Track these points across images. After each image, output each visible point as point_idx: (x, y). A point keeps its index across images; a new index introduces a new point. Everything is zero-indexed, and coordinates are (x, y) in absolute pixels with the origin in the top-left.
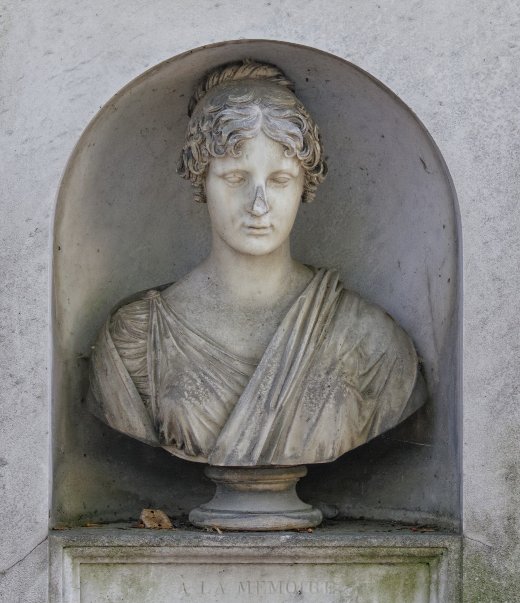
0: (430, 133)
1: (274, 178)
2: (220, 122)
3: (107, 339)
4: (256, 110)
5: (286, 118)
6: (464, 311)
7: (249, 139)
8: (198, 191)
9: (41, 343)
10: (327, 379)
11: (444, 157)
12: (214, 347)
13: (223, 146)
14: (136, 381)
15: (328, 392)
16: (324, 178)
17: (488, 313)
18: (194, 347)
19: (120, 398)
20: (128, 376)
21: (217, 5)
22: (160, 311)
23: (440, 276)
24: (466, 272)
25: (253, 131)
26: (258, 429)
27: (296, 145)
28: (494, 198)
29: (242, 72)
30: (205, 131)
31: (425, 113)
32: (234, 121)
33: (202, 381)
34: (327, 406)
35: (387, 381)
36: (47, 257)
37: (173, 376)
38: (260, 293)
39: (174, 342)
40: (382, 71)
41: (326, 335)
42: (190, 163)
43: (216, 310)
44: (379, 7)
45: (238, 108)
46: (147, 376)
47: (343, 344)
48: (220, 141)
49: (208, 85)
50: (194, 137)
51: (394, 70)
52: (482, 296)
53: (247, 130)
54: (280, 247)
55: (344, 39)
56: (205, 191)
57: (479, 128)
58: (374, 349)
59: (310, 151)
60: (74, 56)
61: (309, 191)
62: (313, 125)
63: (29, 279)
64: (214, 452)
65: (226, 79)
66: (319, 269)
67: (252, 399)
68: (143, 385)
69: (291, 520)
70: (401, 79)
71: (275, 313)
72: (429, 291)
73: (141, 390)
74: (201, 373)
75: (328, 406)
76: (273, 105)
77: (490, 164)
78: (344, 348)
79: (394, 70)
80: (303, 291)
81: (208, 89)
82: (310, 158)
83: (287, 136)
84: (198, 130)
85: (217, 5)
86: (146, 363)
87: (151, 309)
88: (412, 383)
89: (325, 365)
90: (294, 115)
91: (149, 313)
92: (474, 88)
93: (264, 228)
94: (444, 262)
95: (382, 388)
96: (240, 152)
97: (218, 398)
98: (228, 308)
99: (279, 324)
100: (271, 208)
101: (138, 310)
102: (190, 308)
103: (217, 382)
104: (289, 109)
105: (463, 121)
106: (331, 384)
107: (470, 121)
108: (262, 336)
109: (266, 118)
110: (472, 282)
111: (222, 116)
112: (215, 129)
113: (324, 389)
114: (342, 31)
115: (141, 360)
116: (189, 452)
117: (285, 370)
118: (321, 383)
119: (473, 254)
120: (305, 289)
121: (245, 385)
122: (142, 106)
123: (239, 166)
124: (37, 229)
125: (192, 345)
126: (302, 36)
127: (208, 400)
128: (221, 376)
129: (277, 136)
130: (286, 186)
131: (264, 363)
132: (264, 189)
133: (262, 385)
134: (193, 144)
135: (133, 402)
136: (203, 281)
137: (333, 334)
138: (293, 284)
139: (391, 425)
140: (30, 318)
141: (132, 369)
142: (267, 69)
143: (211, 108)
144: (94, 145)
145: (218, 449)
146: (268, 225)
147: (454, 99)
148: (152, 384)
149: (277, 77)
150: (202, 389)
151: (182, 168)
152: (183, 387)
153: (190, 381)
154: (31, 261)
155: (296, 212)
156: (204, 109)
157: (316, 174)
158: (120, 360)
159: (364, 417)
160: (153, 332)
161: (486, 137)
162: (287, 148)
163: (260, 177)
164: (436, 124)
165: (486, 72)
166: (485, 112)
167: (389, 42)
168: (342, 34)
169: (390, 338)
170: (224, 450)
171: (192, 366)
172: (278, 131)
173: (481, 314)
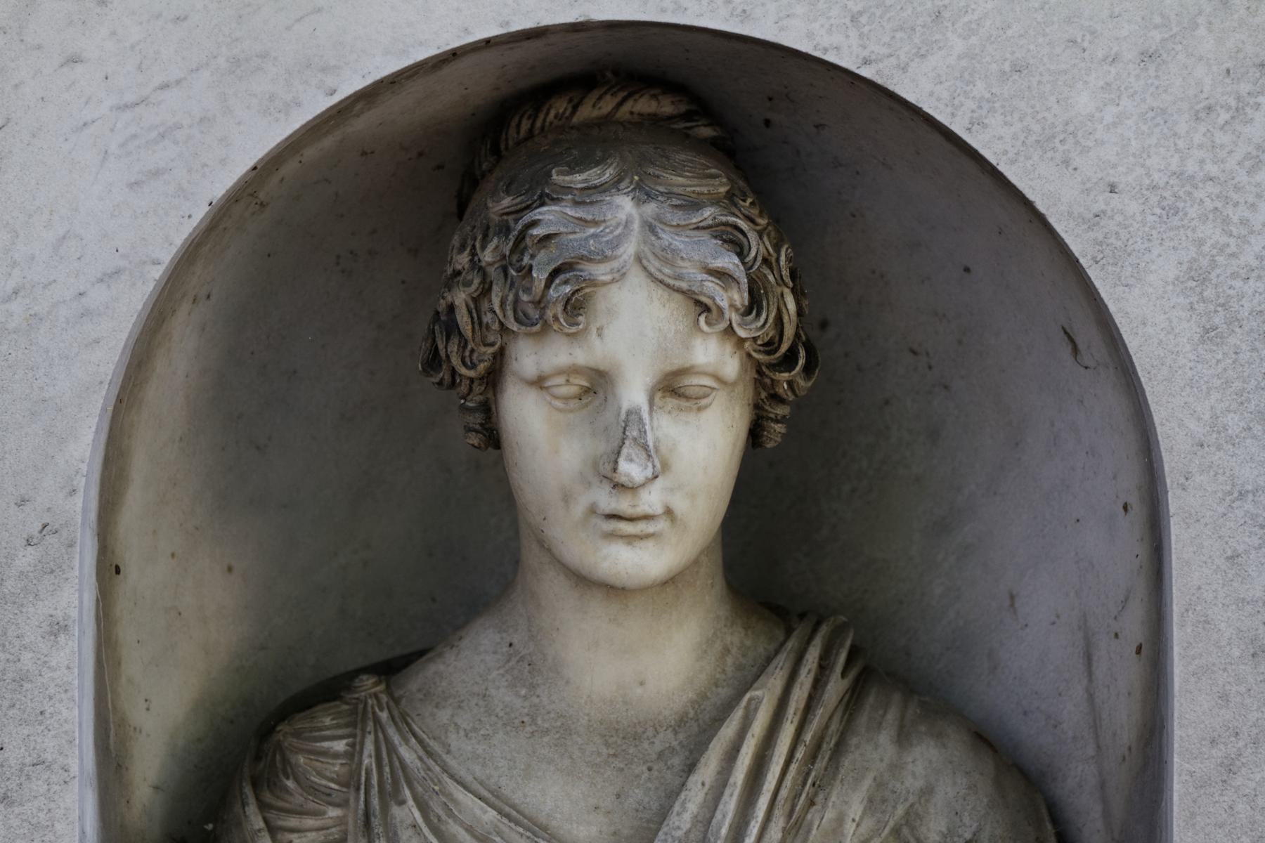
0: (1085, 265)
1: (673, 387)
2: (528, 241)
3: (244, 805)
4: (624, 207)
5: (704, 228)
6: (1176, 738)
7: (605, 284)
8: (476, 419)
9: (58, 826)
11: (1122, 331)
12: (521, 830)
16: (810, 384)
17: (1241, 744)
18: (467, 830)
22: (384, 732)
23: (1116, 635)
24: (1180, 635)
25: (615, 264)
27: (731, 299)
28: (1254, 437)
29: (594, 106)
31: (1070, 214)
32: (564, 238)
36: (74, 596)
38: (642, 684)
39: (417, 814)
40: (956, 102)
41: (816, 794)
42: (454, 347)
43: (528, 729)
45: (577, 204)
47: (862, 818)
48: (528, 290)
49: (507, 140)
50: (461, 278)
52: (1225, 697)
53: (600, 262)
54: (696, 562)
55: (854, 19)
56: (494, 419)
57: (1214, 252)
58: (944, 829)
60: (139, 68)
62: (777, 248)
63: (27, 657)
65: (551, 123)
66: (802, 616)
70: (1006, 124)
71: (681, 736)
72: (1090, 674)
76: (669, 195)
77: (1244, 347)
78: (863, 829)
80: (757, 677)
81: (507, 148)
83: (705, 276)
84: (471, 260)
87: (359, 726)
90: (724, 219)
91: (354, 736)
92: (1200, 146)
93: (647, 518)
94: (1127, 599)
96: (580, 318)
98: (559, 724)
99: (690, 768)
100: (666, 466)
101: (328, 728)
104: (712, 204)
105: (1172, 234)
107: (1189, 233)
108: (647, 799)
109: (650, 228)
110: (1196, 662)
111: (534, 224)
119: (1199, 588)
120: (762, 672)
122: (337, 194)
123: (579, 355)
124: (45, 526)
125: (462, 824)
126: (744, 11)
129: (679, 277)
130: (706, 407)
132: (645, 416)
134: (460, 297)
136: (495, 653)
137: (835, 793)
138: (729, 660)
140: (28, 760)
143: (507, 202)
144: (208, 297)
147: (1148, 175)
149: (687, 116)
151: (434, 361)
154: (31, 610)
155: (735, 473)
157: (786, 375)
160: (363, 787)
161: (1234, 275)
162: (707, 309)
163: (638, 382)
164: (1101, 244)
165: (1233, 103)
166: (1229, 211)
172: (681, 263)
173: (1222, 747)
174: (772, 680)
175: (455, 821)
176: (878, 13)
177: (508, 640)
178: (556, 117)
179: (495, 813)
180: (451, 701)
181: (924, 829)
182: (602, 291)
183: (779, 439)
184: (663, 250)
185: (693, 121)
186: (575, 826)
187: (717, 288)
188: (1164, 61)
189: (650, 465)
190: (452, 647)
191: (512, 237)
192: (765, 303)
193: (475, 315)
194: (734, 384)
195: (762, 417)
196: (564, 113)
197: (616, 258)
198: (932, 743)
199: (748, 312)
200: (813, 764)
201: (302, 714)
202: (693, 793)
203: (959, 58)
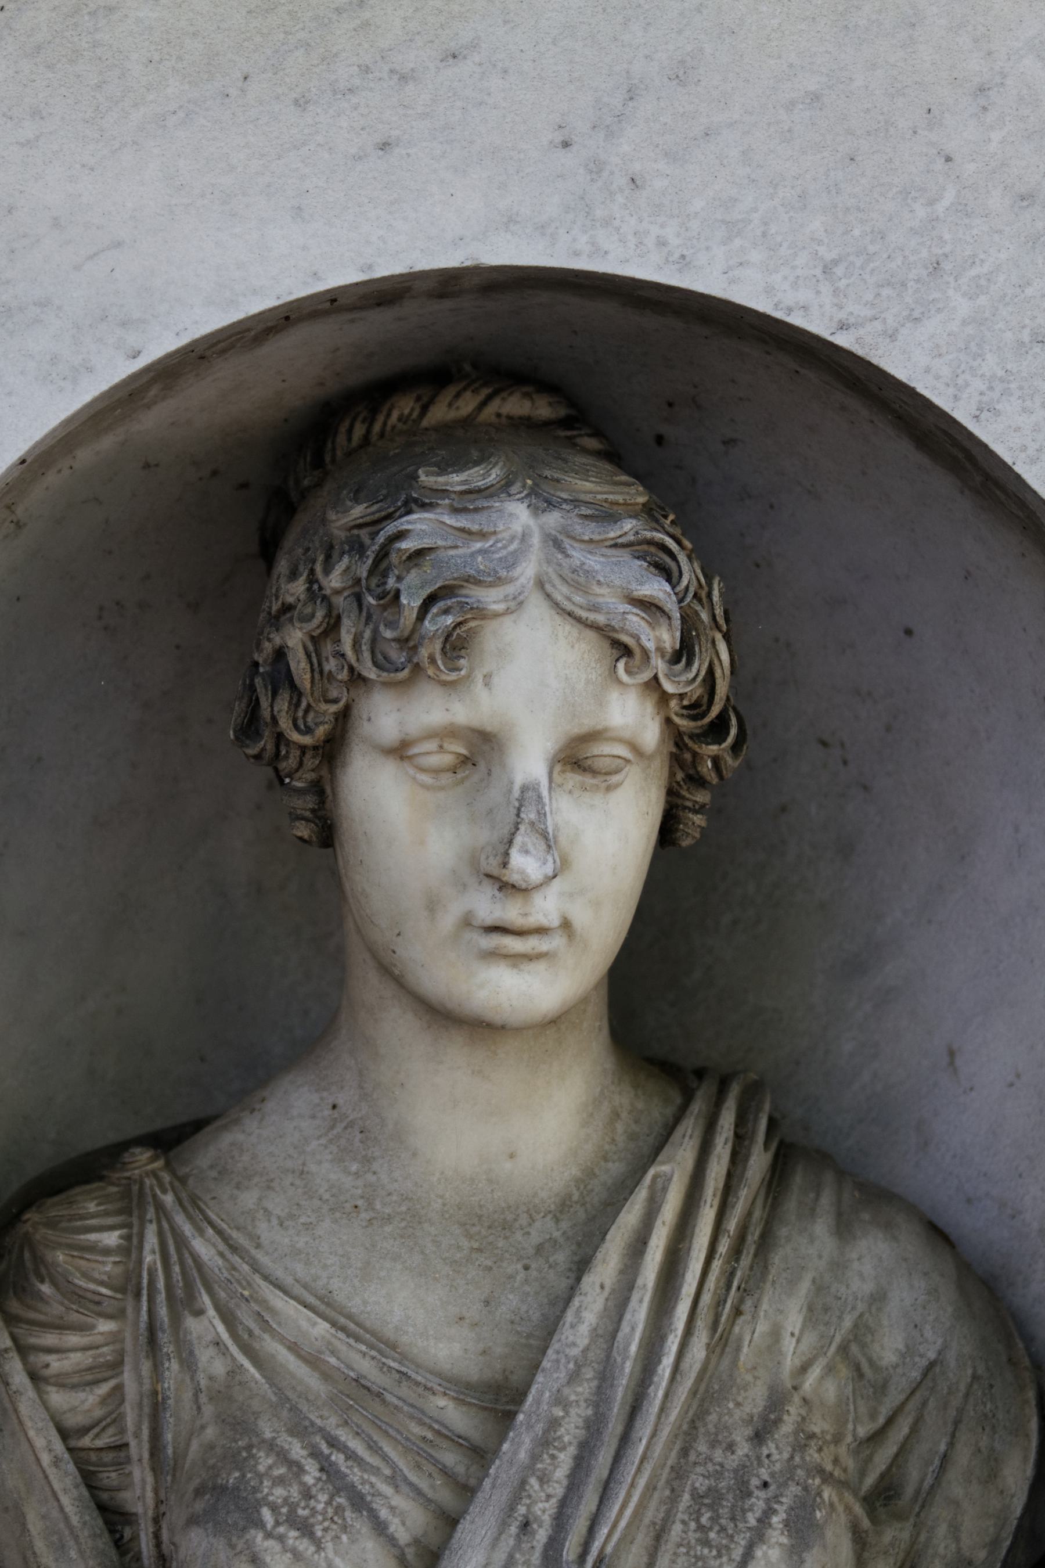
1: (576, 758)
2: (394, 558)
5: (624, 546)
7: (497, 615)
8: (305, 804)
10: (758, 1458)
12: (364, 1348)
13: (403, 642)
14: (88, 1462)
15: (761, 1505)
16: (737, 764)
18: (289, 1348)
19: (30, 1527)
20: (59, 1446)
21: (384, 146)
22: (169, 1220)
25: (510, 589)
29: (450, 405)
30: (337, 592)
32: (442, 554)
33: (322, 1469)
34: (759, 1553)
35: (945, 1458)
37: (219, 1451)
38: (512, 1156)
39: (221, 1328)
40: (960, 381)
41: (741, 1301)
42: (283, 704)
43: (364, 1215)
44: (948, 159)
45: (456, 511)
46: (126, 1445)
49: (334, 449)
51: (1002, 380)
53: (491, 585)
54: (584, 1000)
55: (827, 270)
56: (327, 806)
58: (901, 1346)
59: (699, 667)
61: (685, 808)
65: (394, 427)
66: (700, 1074)
67: (500, 1534)
68: (110, 1477)
70: (1024, 410)
71: (565, 1225)
73: (105, 1496)
74: (318, 1439)
75: (765, 1554)
76: (576, 502)
78: (804, 1346)
79: (1002, 380)
81: (333, 461)
82: (695, 691)
83: (628, 608)
84: (309, 589)
85: (384, 146)
87: (136, 1213)
88: (1025, 1459)
89: (748, 1410)
90: (648, 535)
91: (129, 1226)
93: (541, 931)
95: (929, 1480)
96: (462, 661)
97: (380, 1528)
98: (404, 1208)
99: (582, 1266)
101: (93, 1216)
102: (270, 1206)
103: (376, 1471)
104: (630, 517)
106: (772, 1475)
108: (524, 1308)
109: (555, 542)
111: (401, 535)
112: (374, 581)
113: (750, 1494)
114: (820, 242)
115: (104, 1389)
117: (614, 1427)
118: (735, 1471)
121: (472, 1482)
125: (282, 1340)
126: (683, 257)
128: (387, 1448)
129: (595, 608)
130: (617, 786)
131: (538, 1402)
132: (545, 793)
133: (533, 1481)
135: (76, 1538)
136: (313, 1117)
137: (765, 1299)
138: (620, 1127)
141: (72, 1421)
142: (534, 396)
143: (358, 511)
146: (553, 920)
148: (141, 1474)
149: (566, 423)
150: (323, 1498)
151: (251, 725)
152: (255, 1490)
153: (281, 1471)
156: (332, 516)
158: (31, 1393)
160: (145, 1292)
167: (983, 282)
168: (822, 250)
169: (950, 1309)
171: (285, 1414)
172: (597, 590)
174: (681, 1152)
175: (273, 1337)
176: (858, 262)
177: (331, 1101)
178: (400, 419)
179: (327, 1326)
180: (256, 1179)
181: (876, 1347)
182: (491, 625)
183: (698, 835)
184: (574, 571)
185: (572, 428)
186: (432, 1342)
187: (643, 624)
189: (550, 859)
190: (253, 1111)
191: (371, 555)
192: (697, 649)
193: (315, 660)
194: (650, 758)
195: (677, 806)
196: (410, 414)
197: (511, 580)
198: (881, 1235)
199: (676, 658)
200: (737, 1260)
201: (56, 1199)
202: (589, 1298)
203: (964, 323)
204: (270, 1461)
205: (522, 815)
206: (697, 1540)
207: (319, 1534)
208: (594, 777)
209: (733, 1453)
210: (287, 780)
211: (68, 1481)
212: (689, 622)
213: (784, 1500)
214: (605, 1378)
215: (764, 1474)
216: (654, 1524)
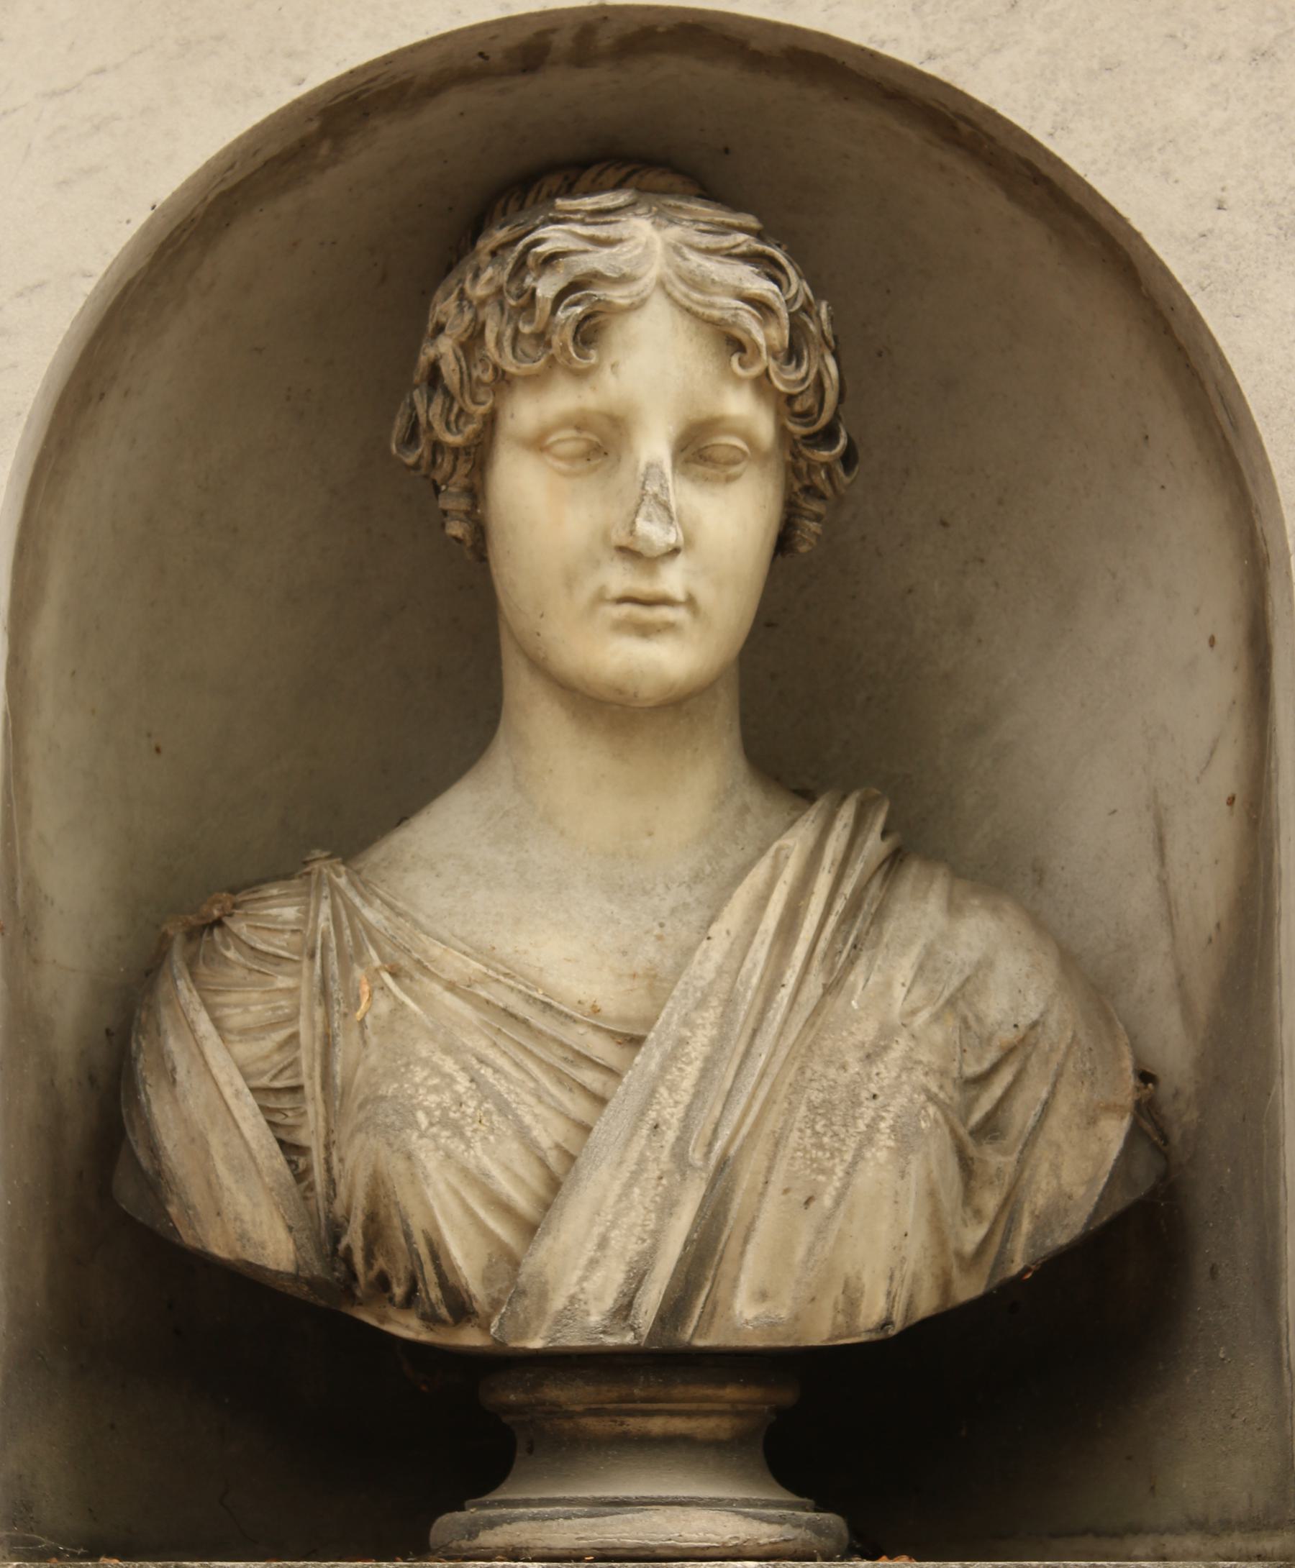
1: (698, 448)
2: (531, 261)
19: (213, 1152)
20: (240, 1082)
26: (651, 1226)
33: (472, 1080)
47: (913, 982)
64: (510, 1303)
67: (633, 1135)
69: (756, 1524)
86: (298, 1047)
93: (666, 601)
96: (593, 352)
106: (881, 1088)
113: (860, 1104)
116: (432, 1306)
127: (492, 1138)
131: (668, 1024)
139: (1062, 1237)
145: (522, 1293)
146: (680, 595)
147: (1262, 189)
150: (473, 1103)
153: (436, 1081)
155: (760, 592)
159: (978, 1213)
164: (1207, 268)
170: (543, 1296)
188: (1279, 61)
192: (805, 353)
204: (425, 1074)
205: (648, 488)
206: (812, 1145)
207: (469, 1134)
208: (714, 467)
209: (846, 1070)
210: (443, 488)
211: (247, 1112)
212: (797, 328)
213: (891, 1109)
214: (730, 1002)
215: (874, 1088)
216: (774, 1132)
